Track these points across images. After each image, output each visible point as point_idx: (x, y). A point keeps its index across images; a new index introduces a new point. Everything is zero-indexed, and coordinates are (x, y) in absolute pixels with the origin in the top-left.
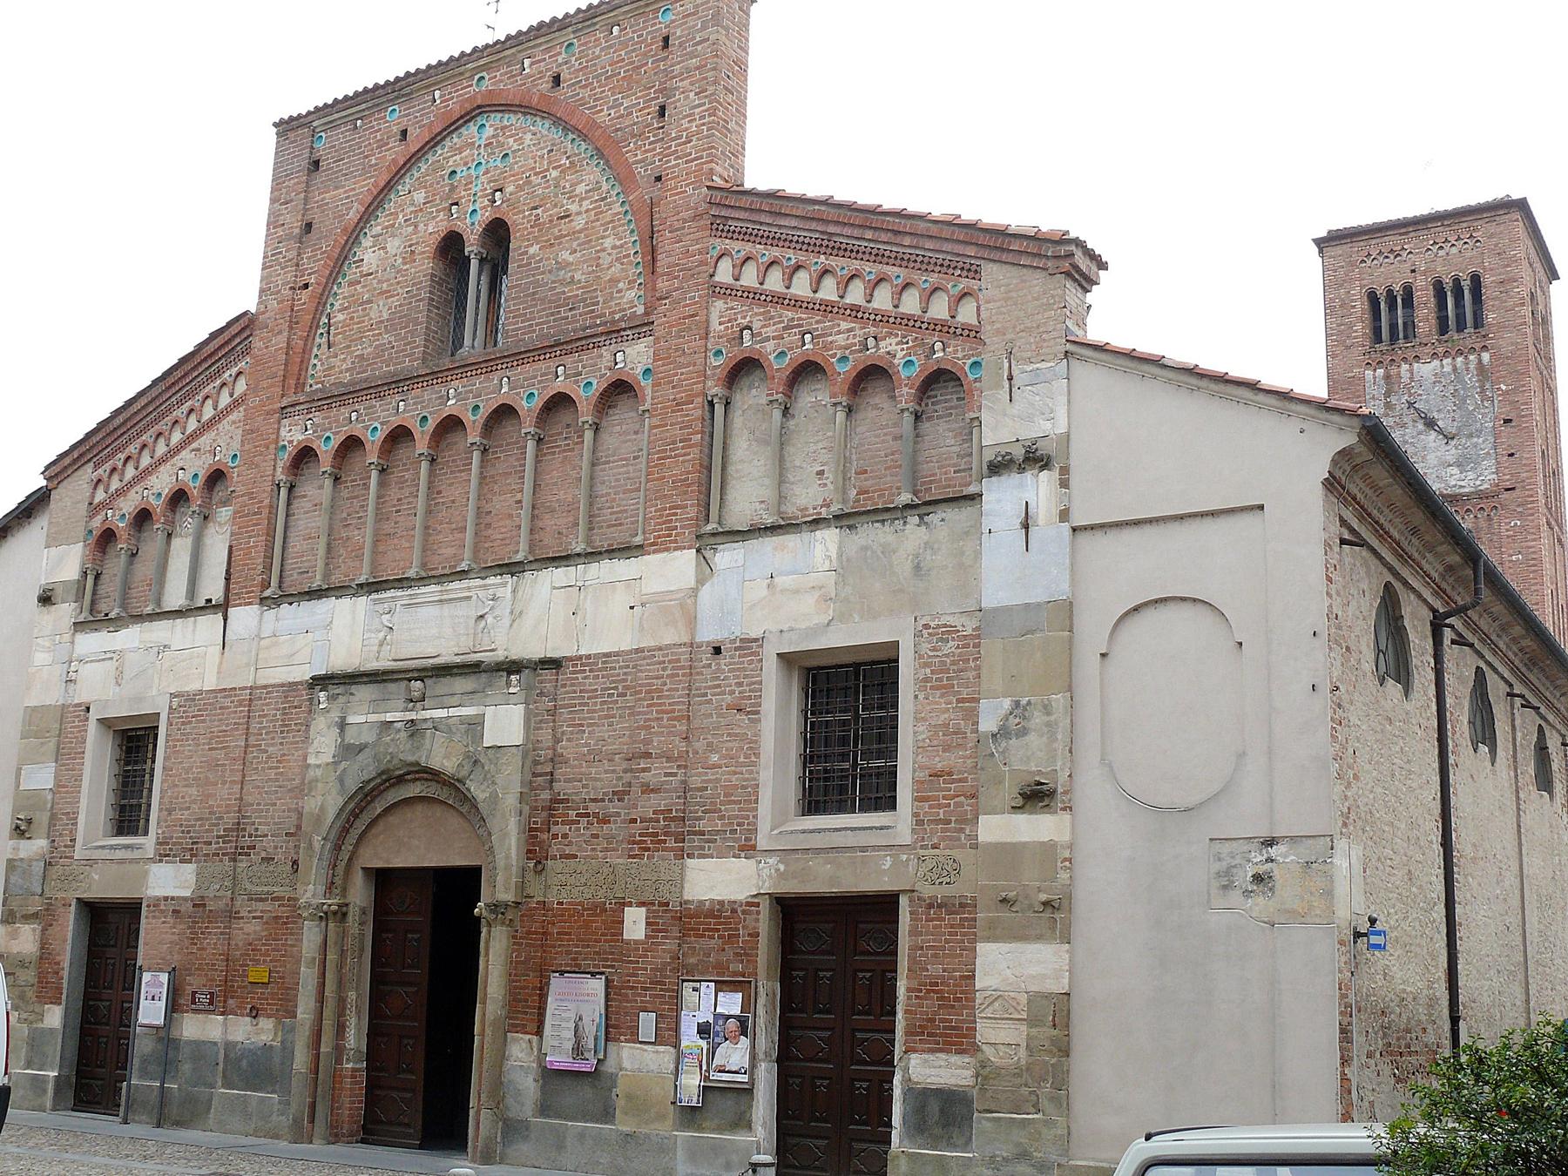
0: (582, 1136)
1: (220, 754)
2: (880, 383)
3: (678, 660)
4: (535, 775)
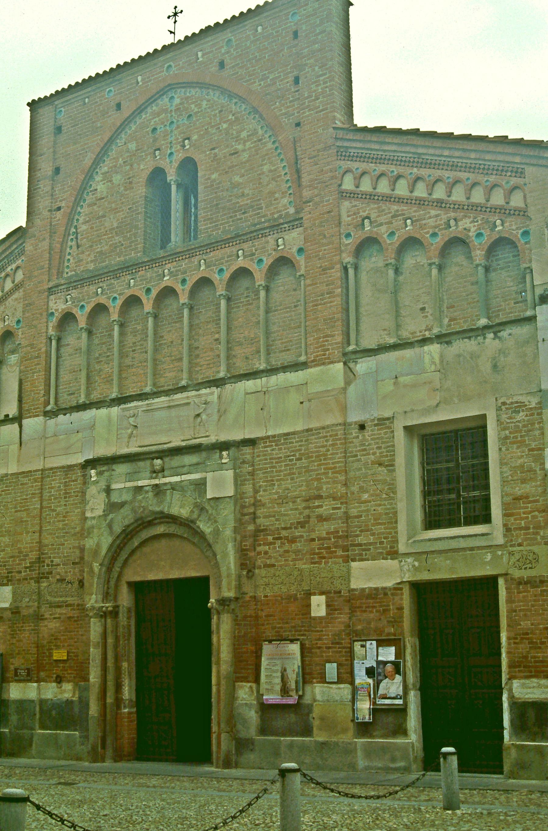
0: (291, 746)
1: (24, 514)
2: (376, 247)
3: (337, 435)
4: (244, 515)
